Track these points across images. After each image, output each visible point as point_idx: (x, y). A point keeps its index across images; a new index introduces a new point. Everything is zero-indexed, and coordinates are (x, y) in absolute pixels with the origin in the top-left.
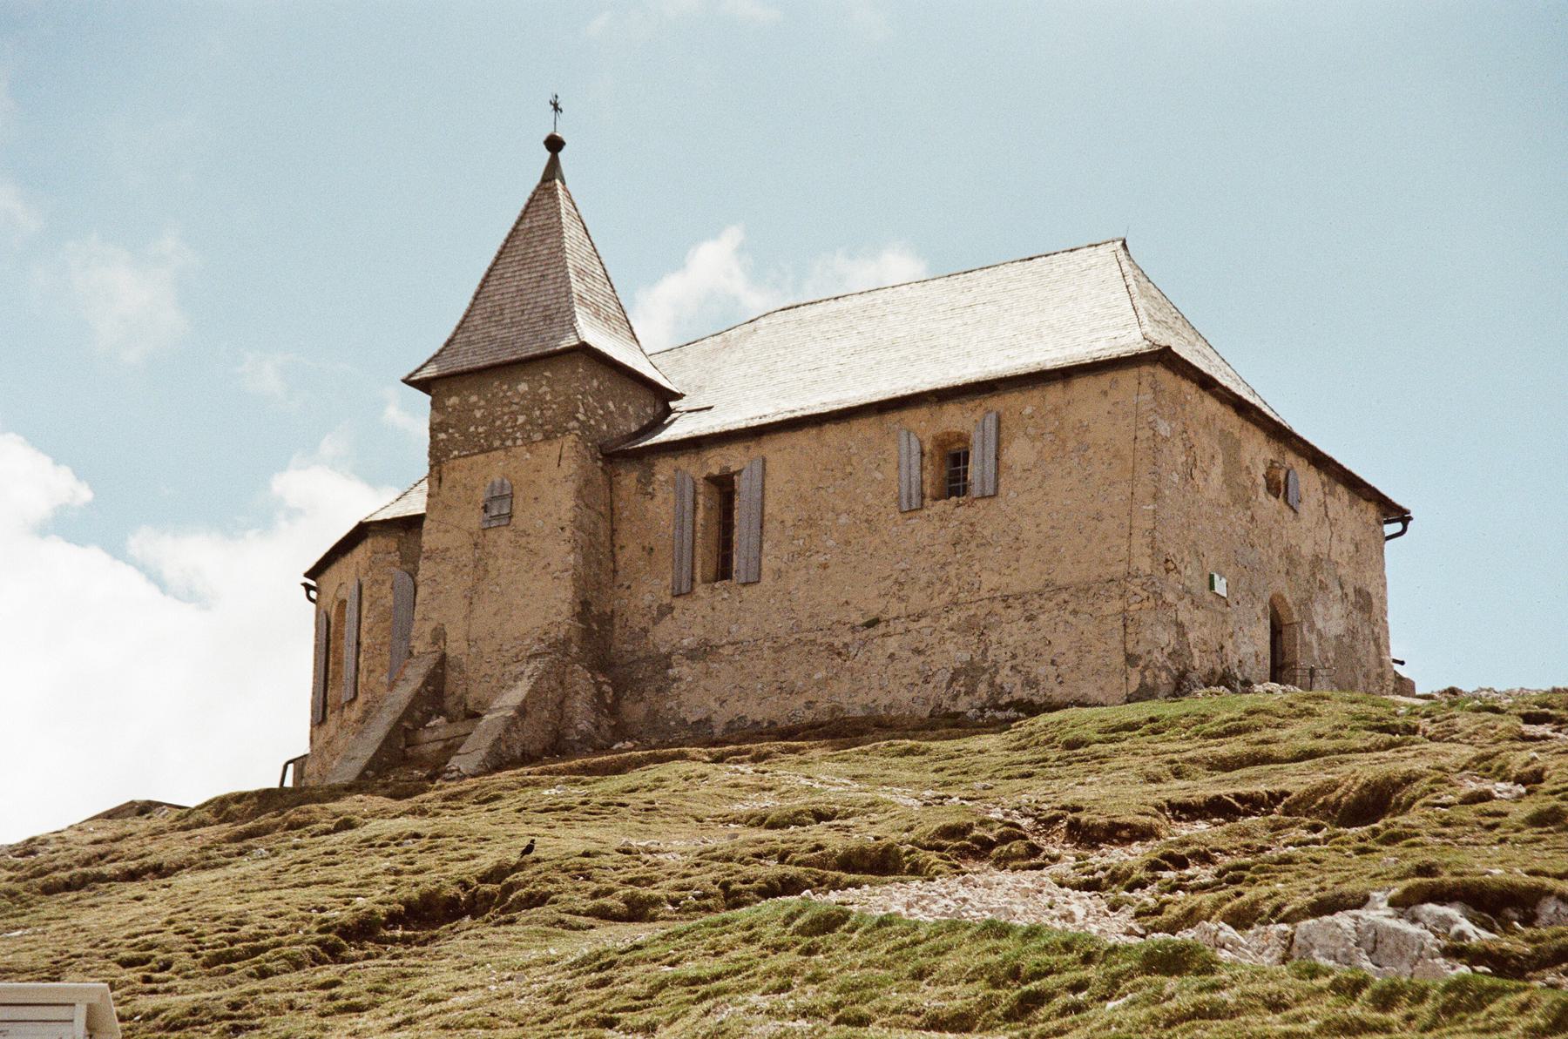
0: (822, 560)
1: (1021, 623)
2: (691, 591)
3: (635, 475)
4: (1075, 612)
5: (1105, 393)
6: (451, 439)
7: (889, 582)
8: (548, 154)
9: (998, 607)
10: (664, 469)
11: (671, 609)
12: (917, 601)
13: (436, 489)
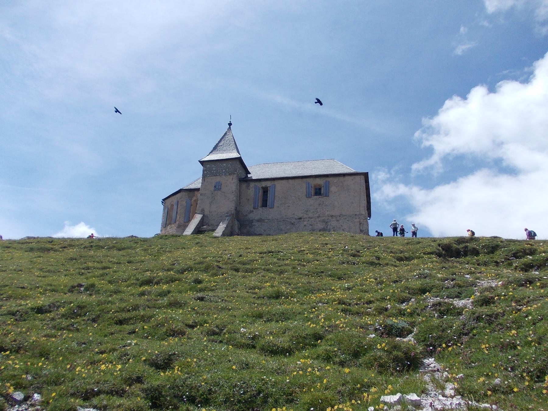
0: (288, 205)
1: (335, 221)
2: (258, 208)
3: (245, 185)
4: (348, 221)
5: (353, 180)
6: (207, 173)
7: (304, 211)
8: (229, 126)
9: (330, 218)
10: (252, 185)
11: (253, 211)
12: (310, 215)
13: (203, 182)
